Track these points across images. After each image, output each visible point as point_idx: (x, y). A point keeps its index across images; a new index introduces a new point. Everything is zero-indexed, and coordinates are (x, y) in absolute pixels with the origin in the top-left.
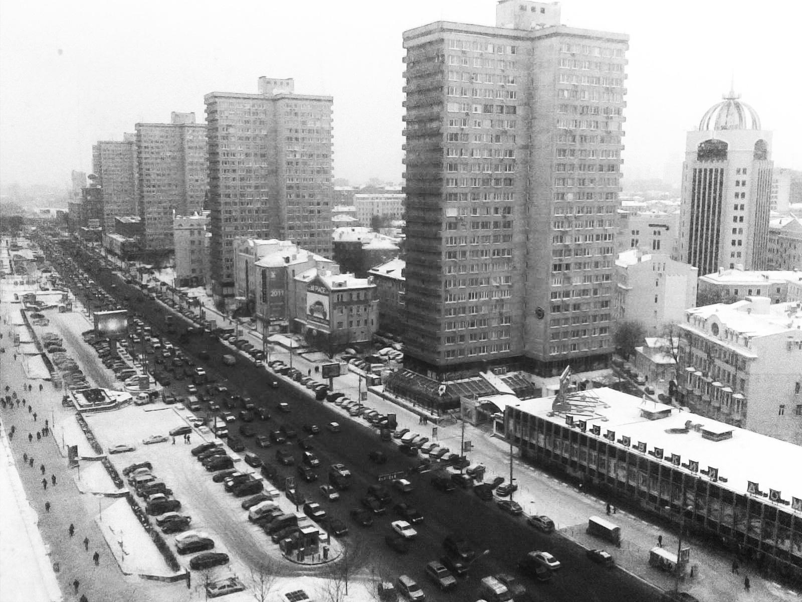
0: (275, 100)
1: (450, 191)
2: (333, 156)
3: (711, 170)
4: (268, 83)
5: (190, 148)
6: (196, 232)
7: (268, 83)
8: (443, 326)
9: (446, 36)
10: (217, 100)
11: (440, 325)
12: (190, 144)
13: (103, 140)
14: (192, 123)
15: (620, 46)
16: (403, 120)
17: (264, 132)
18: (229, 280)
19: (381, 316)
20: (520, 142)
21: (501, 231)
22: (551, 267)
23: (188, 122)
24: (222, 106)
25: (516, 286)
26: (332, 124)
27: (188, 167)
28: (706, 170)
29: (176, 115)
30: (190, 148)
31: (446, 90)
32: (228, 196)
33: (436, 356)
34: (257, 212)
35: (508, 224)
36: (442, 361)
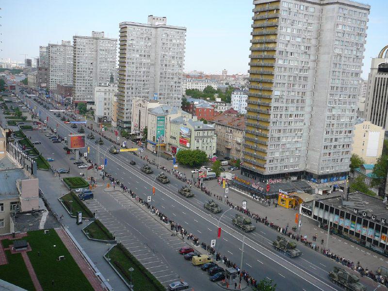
0: (157, 28)
1: (277, 81)
2: (184, 58)
3: (379, 78)
4: (154, 19)
5: (100, 50)
6: (108, 93)
7: (154, 19)
8: (268, 154)
9: (127, 26)
10: (127, 26)
11: (266, 153)
12: (101, 48)
13: (52, 43)
14: (103, 37)
15: (365, 12)
16: (251, 42)
17: (150, 44)
18: (128, 120)
19: (218, 144)
20: (312, 58)
21: (300, 105)
22: (326, 125)
23: (100, 37)
24: (78, 40)
25: (304, 134)
26: (185, 42)
27: (99, 60)
28: (379, 78)
29: (95, 33)
30: (100, 50)
31: (279, 28)
32: (130, 76)
33: (263, 170)
34: (89, 80)
35: (303, 101)
36: (267, 172)
